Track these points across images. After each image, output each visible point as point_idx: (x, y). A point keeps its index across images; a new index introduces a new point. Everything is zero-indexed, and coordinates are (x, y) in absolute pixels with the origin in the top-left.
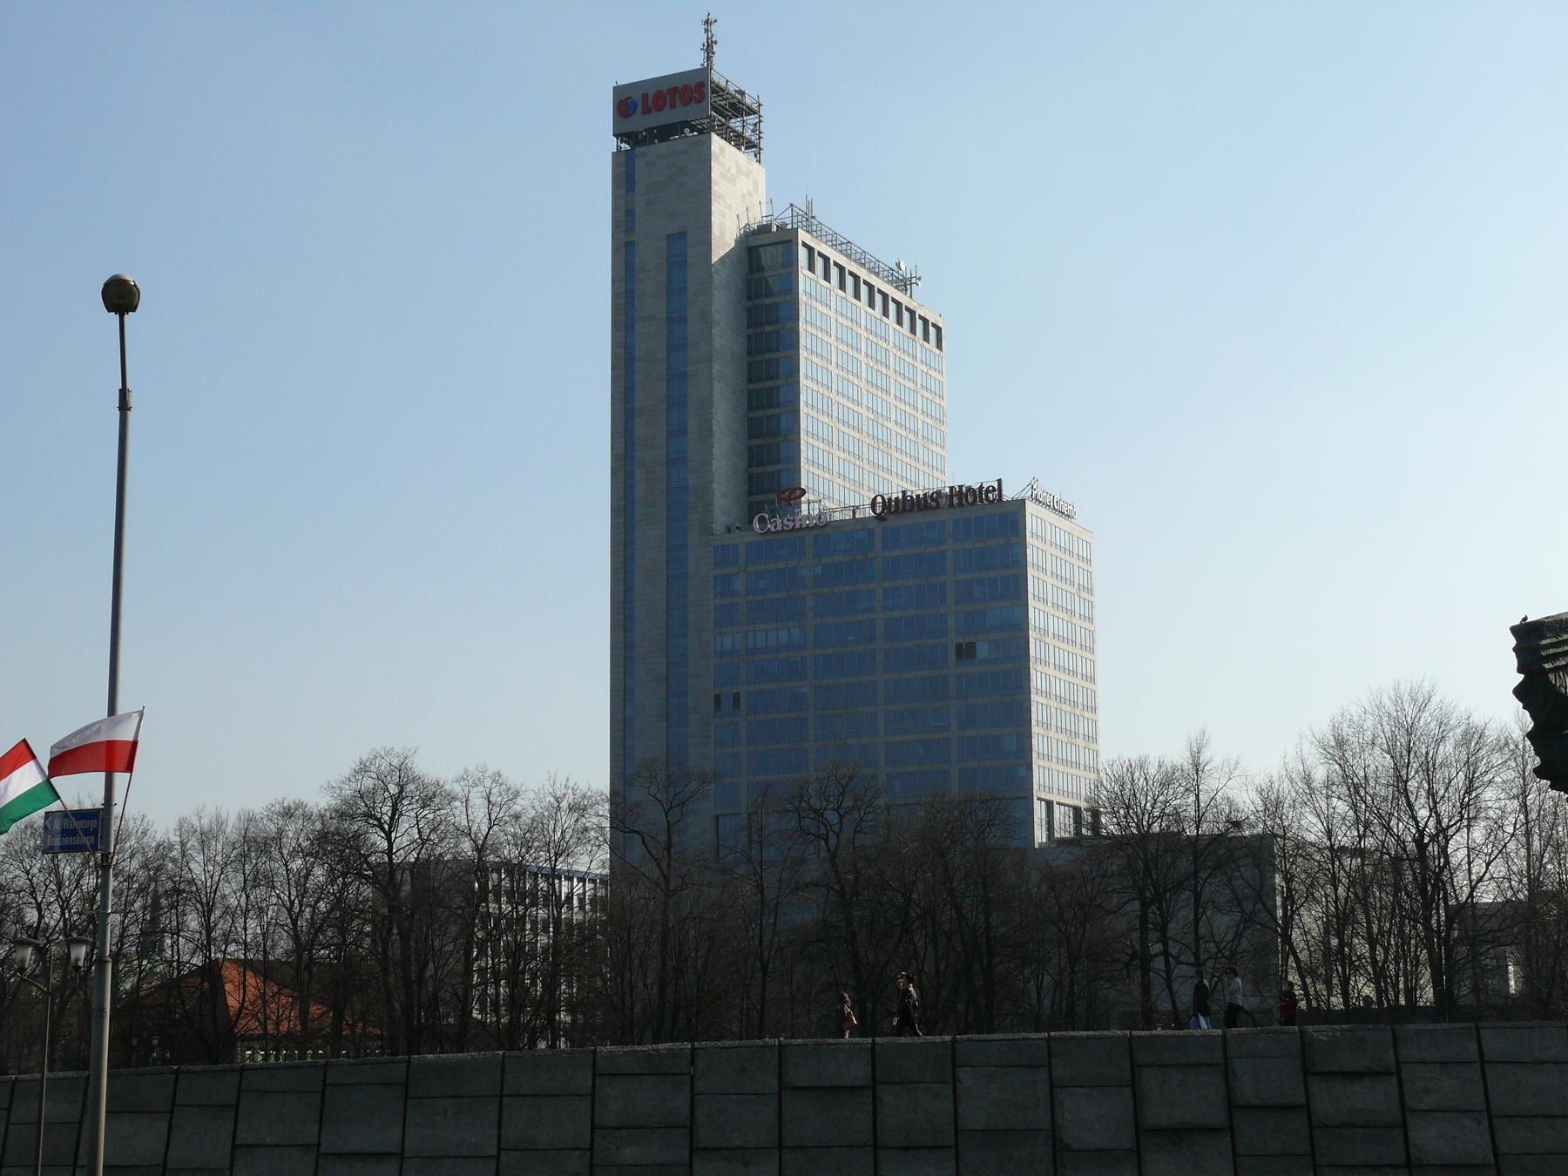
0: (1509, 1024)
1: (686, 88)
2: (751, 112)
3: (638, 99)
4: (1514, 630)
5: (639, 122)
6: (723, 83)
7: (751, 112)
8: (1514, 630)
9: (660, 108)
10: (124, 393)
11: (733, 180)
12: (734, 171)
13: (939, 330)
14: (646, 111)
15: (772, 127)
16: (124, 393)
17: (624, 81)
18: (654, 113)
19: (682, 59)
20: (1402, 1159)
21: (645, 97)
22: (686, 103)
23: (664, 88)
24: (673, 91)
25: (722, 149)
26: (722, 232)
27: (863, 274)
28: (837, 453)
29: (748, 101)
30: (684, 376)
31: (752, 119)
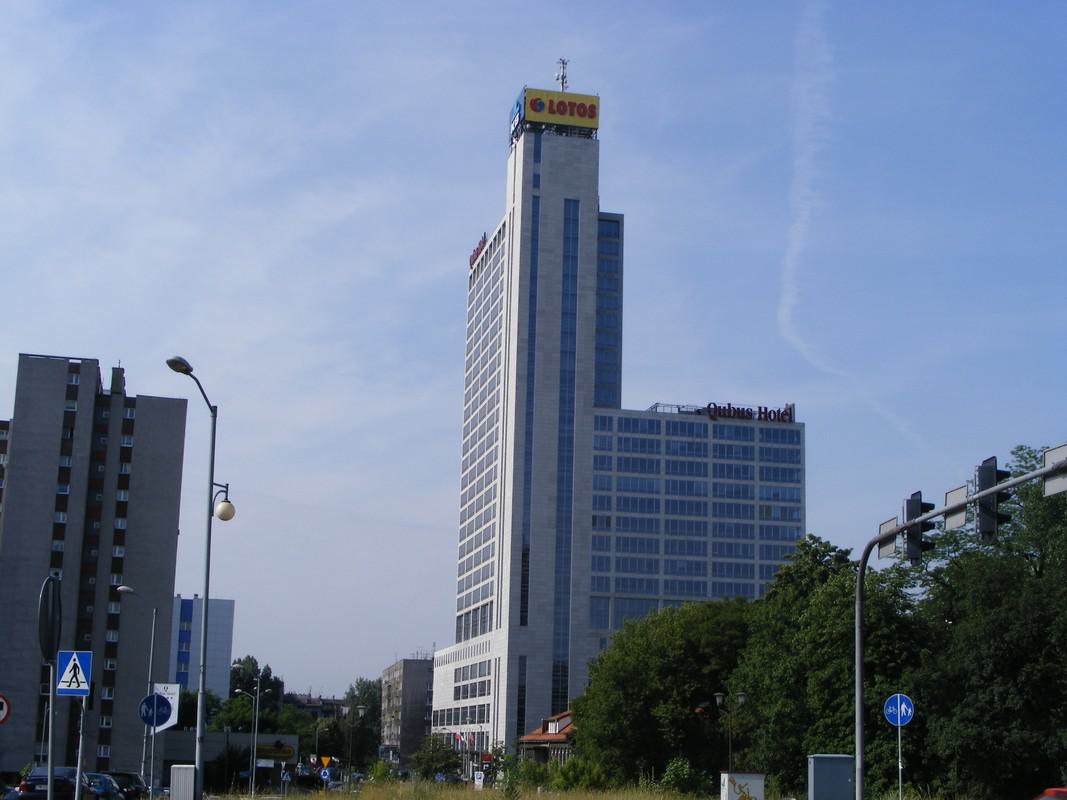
9: (562, 113)
14: (551, 111)
24: (572, 105)
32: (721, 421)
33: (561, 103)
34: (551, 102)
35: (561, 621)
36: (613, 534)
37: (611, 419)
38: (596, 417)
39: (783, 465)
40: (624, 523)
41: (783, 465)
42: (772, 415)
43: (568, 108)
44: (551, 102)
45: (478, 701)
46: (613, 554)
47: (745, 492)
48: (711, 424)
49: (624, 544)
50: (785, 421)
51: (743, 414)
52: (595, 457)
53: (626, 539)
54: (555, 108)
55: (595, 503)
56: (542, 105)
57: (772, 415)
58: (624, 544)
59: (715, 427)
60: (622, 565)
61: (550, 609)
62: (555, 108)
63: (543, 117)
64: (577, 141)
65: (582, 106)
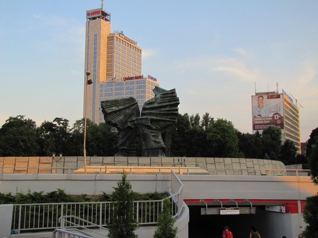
0: (175, 167)
1: (97, 12)
2: (109, 15)
3: (90, 13)
4: (173, 92)
5: (91, 17)
6: (107, 13)
7: (109, 15)
8: (173, 92)
9: (93, 14)
10: (277, 86)
11: (105, 26)
12: (105, 25)
13: (141, 50)
14: (91, 15)
15: (112, 18)
16: (277, 86)
17: (88, 10)
18: (93, 15)
19: (95, 6)
20: (241, 164)
21: (91, 13)
22: (97, 14)
23: (94, 11)
24: (96, 12)
25: (103, 21)
26: (103, 34)
27: (129, 43)
28: (121, 70)
29: (108, 13)
30: (96, 57)
31: (109, 17)
59: (125, 82)
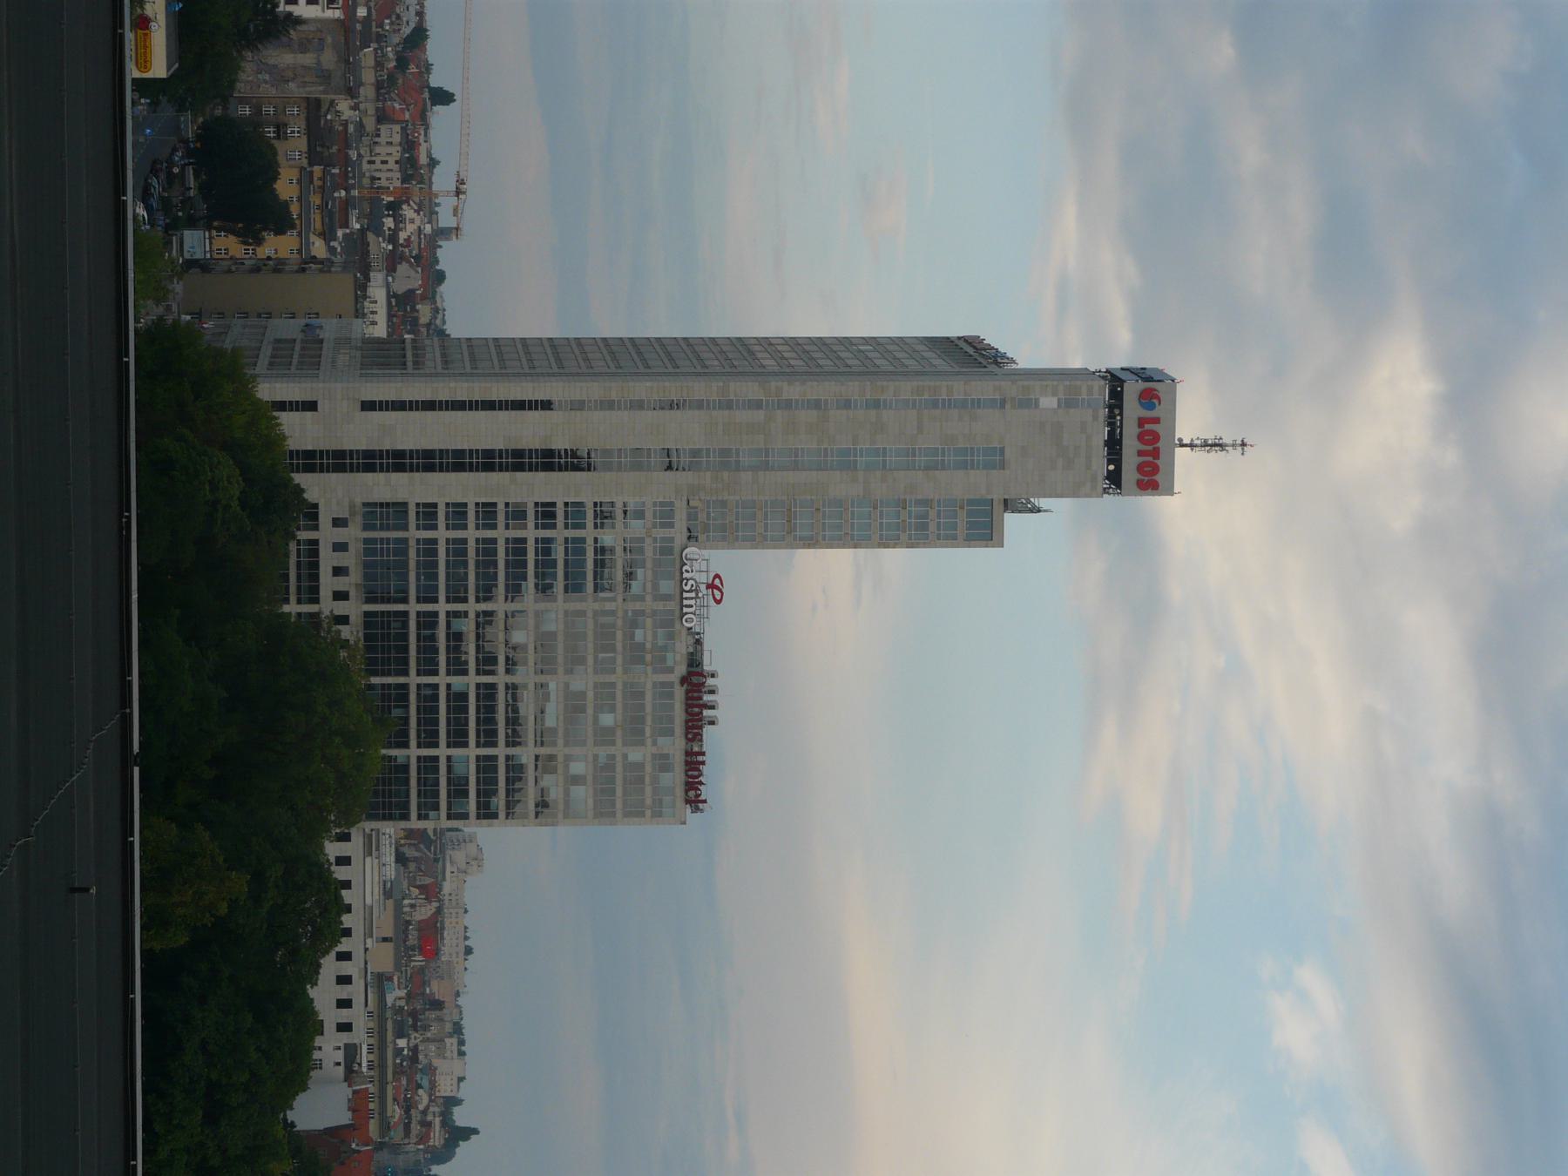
9: (1141, 437)
14: (1142, 422)
22: (1140, 468)
24: (1156, 453)
32: (679, 693)
33: (1156, 437)
34: (1156, 421)
35: (370, 461)
36: (531, 533)
37: (671, 525)
38: (671, 504)
39: (619, 792)
40: (458, 548)
41: (619, 792)
42: (696, 773)
43: (1150, 448)
44: (1156, 421)
45: (410, 364)
46: (500, 534)
47: (458, 738)
48: (675, 677)
49: (517, 548)
50: (686, 792)
51: (693, 727)
52: (405, 504)
53: (524, 552)
54: (1147, 427)
55: (426, 505)
56: (1151, 407)
57: (696, 773)
58: (517, 548)
59: (671, 685)
60: (487, 547)
61: (387, 445)
62: (1147, 427)
63: (1132, 409)
64: (1101, 466)
65: (1156, 469)
